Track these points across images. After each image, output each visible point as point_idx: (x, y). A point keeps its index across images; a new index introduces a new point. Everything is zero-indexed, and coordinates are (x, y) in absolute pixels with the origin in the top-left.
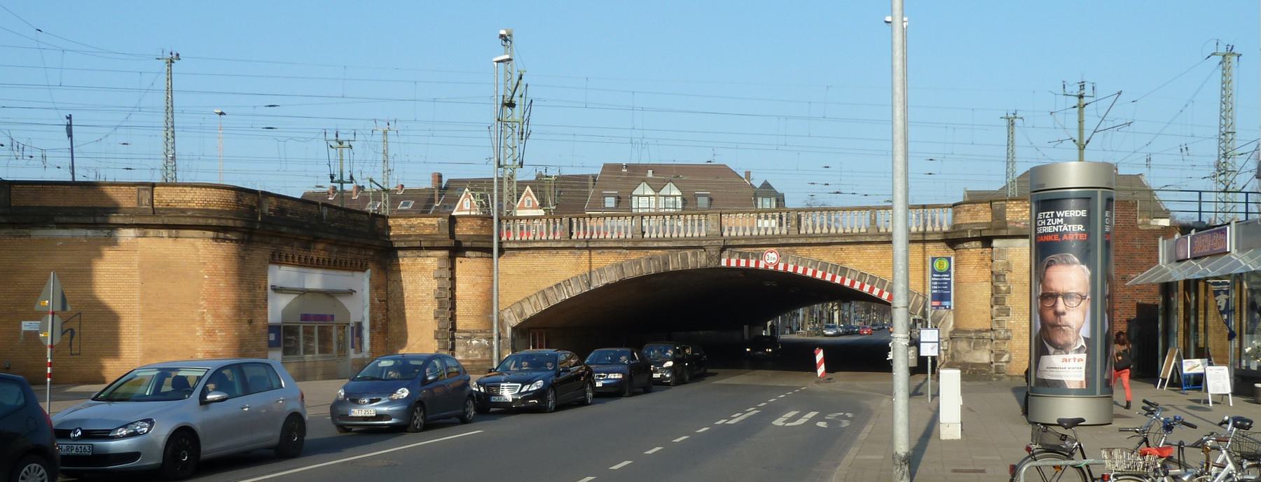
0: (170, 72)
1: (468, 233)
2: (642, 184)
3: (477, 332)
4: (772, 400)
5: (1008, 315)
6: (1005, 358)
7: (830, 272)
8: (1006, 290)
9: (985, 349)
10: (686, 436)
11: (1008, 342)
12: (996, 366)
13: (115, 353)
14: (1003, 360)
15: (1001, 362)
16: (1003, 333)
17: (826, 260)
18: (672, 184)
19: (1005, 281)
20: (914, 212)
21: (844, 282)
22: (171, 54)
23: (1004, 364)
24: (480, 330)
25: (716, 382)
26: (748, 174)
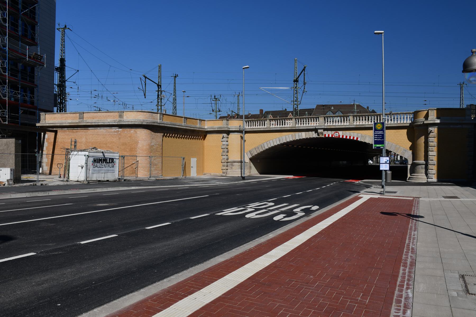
0: (175, 80)
2: (338, 112)
13: (39, 121)
18: (330, 112)
20: (396, 115)
21: (358, 139)
22: (176, 75)
25: (347, 181)
26: (368, 108)
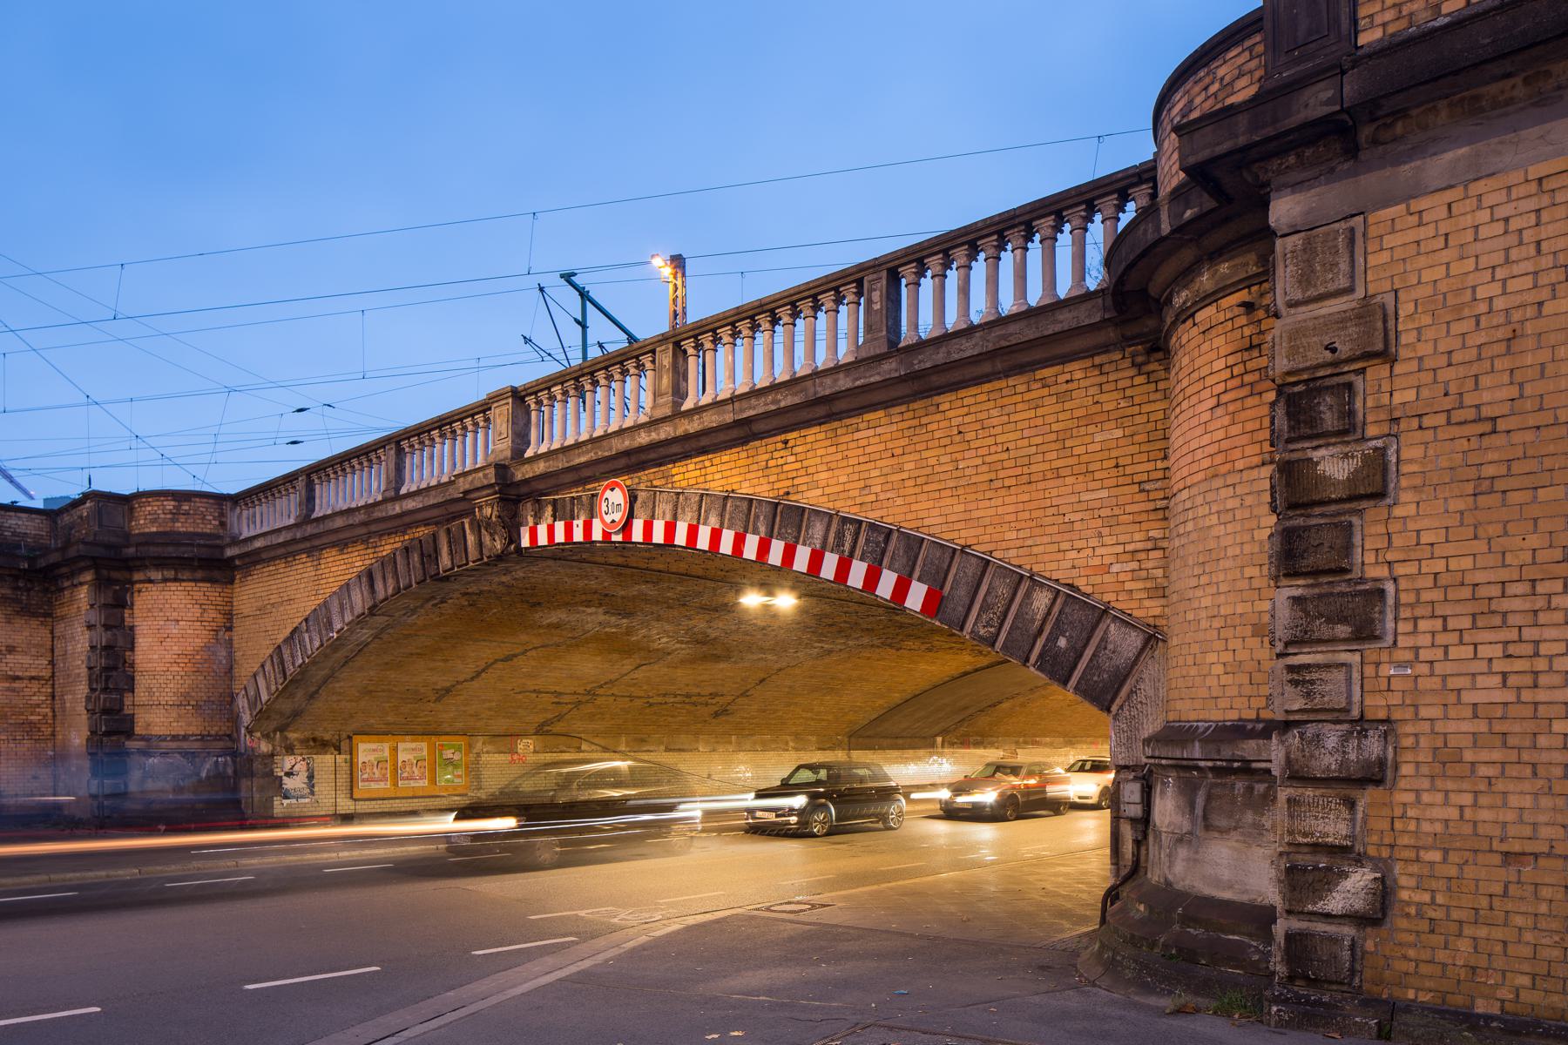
1: (147, 530)
3: (165, 740)
4: (736, 1033)
5: (1365, 633)
6: (1353, 889)
7: (755, 532)
8: (1353, 479)
9: (1259, 828)
10: (248, 990)
11: (1366, 798)
12: (1290, 937)
14: (1335, 903)
15: (1328, 917)
16: (1332, 741)
17: (745, 489)
19: (1349, 429)
23: (1348, 931)
24: (174, 736)
